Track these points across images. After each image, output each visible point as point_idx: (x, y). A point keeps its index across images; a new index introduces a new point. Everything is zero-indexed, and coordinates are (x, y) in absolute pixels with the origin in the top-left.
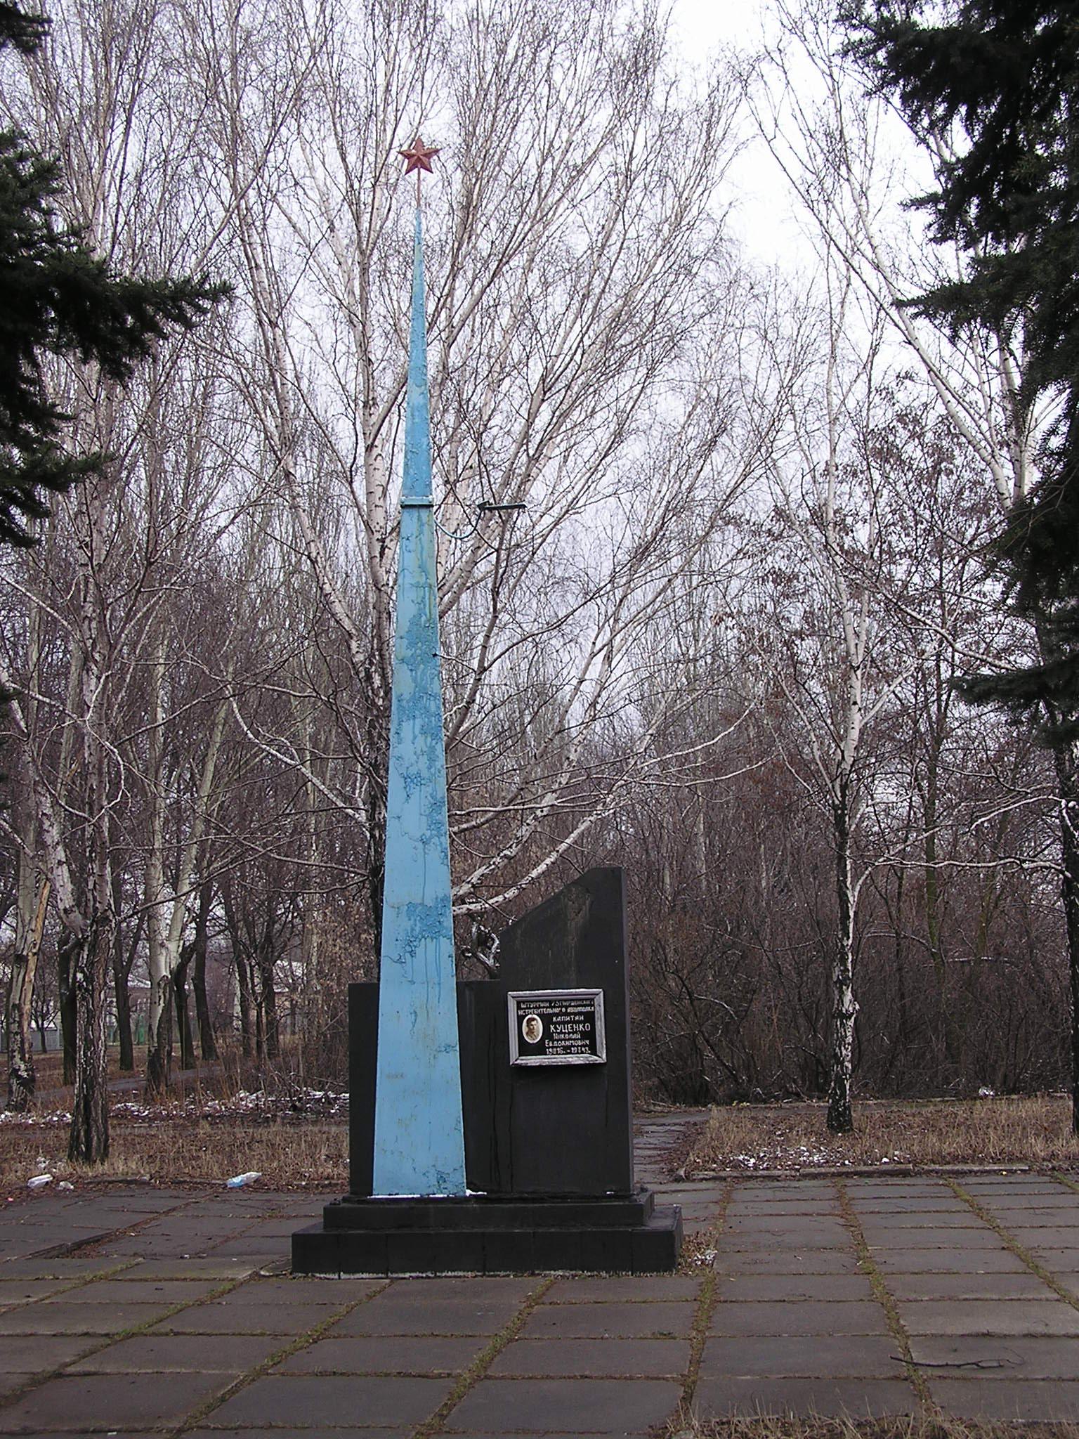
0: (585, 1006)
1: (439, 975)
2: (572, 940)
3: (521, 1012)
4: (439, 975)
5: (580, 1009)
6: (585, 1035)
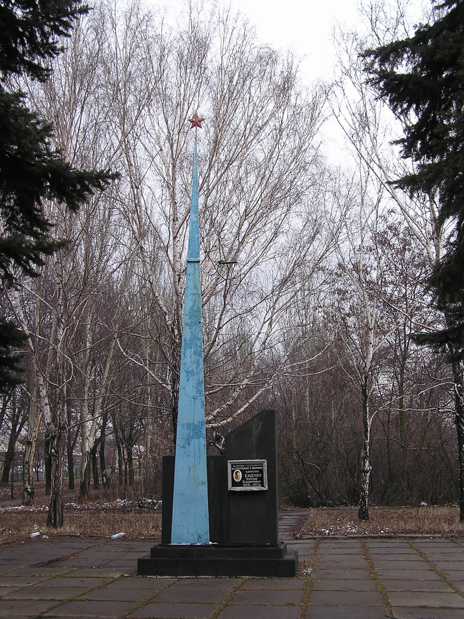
1: (200, 453)
2: (254, 440)
3: (233, 469)
4: (200, 453)
5: (257, 468)
6: (259, 479)
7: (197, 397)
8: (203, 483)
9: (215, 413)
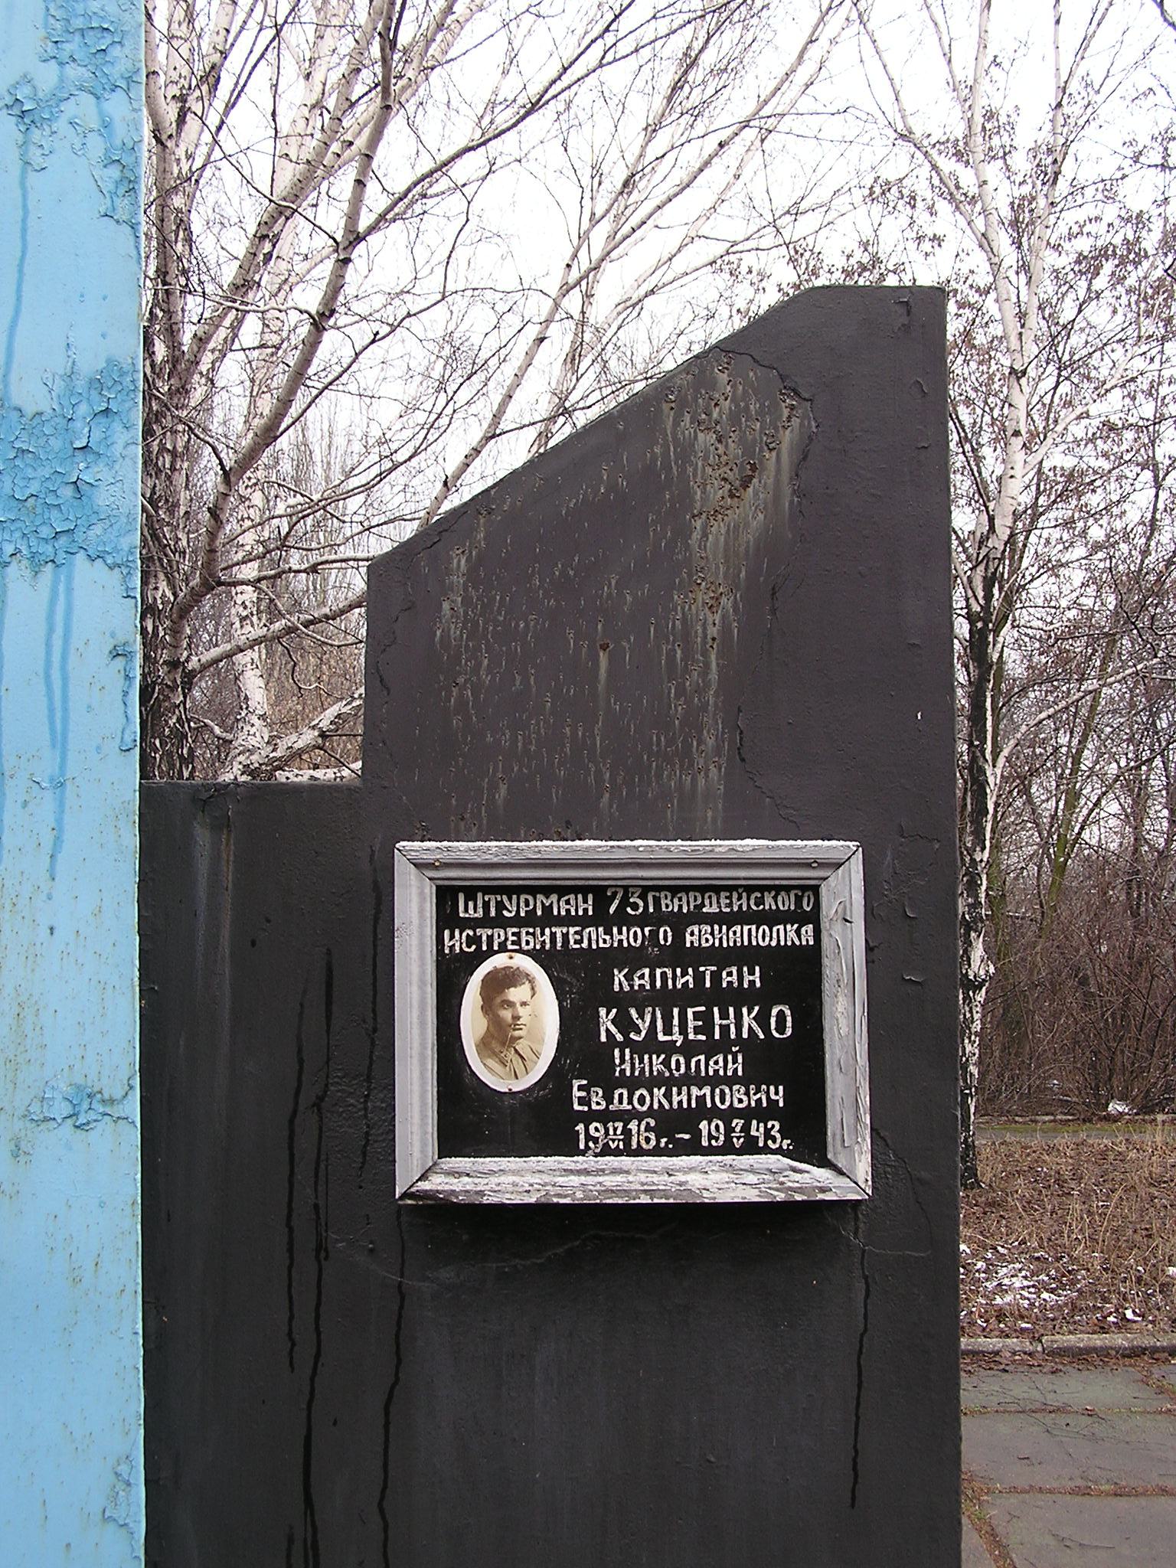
0: (772, 919)
1: (60, 741)
2: (710, 612)
3: (457, 942)
4: (60, 741)
5: (741, 935)
6: (762, 1061)
7: (59, 98)
8: (84, 1107)
9: (325, 719)
